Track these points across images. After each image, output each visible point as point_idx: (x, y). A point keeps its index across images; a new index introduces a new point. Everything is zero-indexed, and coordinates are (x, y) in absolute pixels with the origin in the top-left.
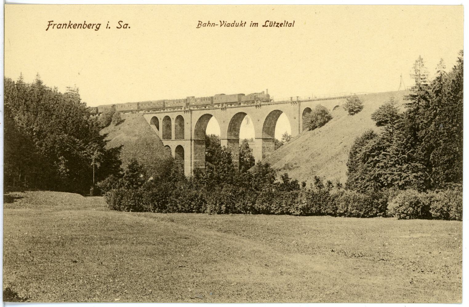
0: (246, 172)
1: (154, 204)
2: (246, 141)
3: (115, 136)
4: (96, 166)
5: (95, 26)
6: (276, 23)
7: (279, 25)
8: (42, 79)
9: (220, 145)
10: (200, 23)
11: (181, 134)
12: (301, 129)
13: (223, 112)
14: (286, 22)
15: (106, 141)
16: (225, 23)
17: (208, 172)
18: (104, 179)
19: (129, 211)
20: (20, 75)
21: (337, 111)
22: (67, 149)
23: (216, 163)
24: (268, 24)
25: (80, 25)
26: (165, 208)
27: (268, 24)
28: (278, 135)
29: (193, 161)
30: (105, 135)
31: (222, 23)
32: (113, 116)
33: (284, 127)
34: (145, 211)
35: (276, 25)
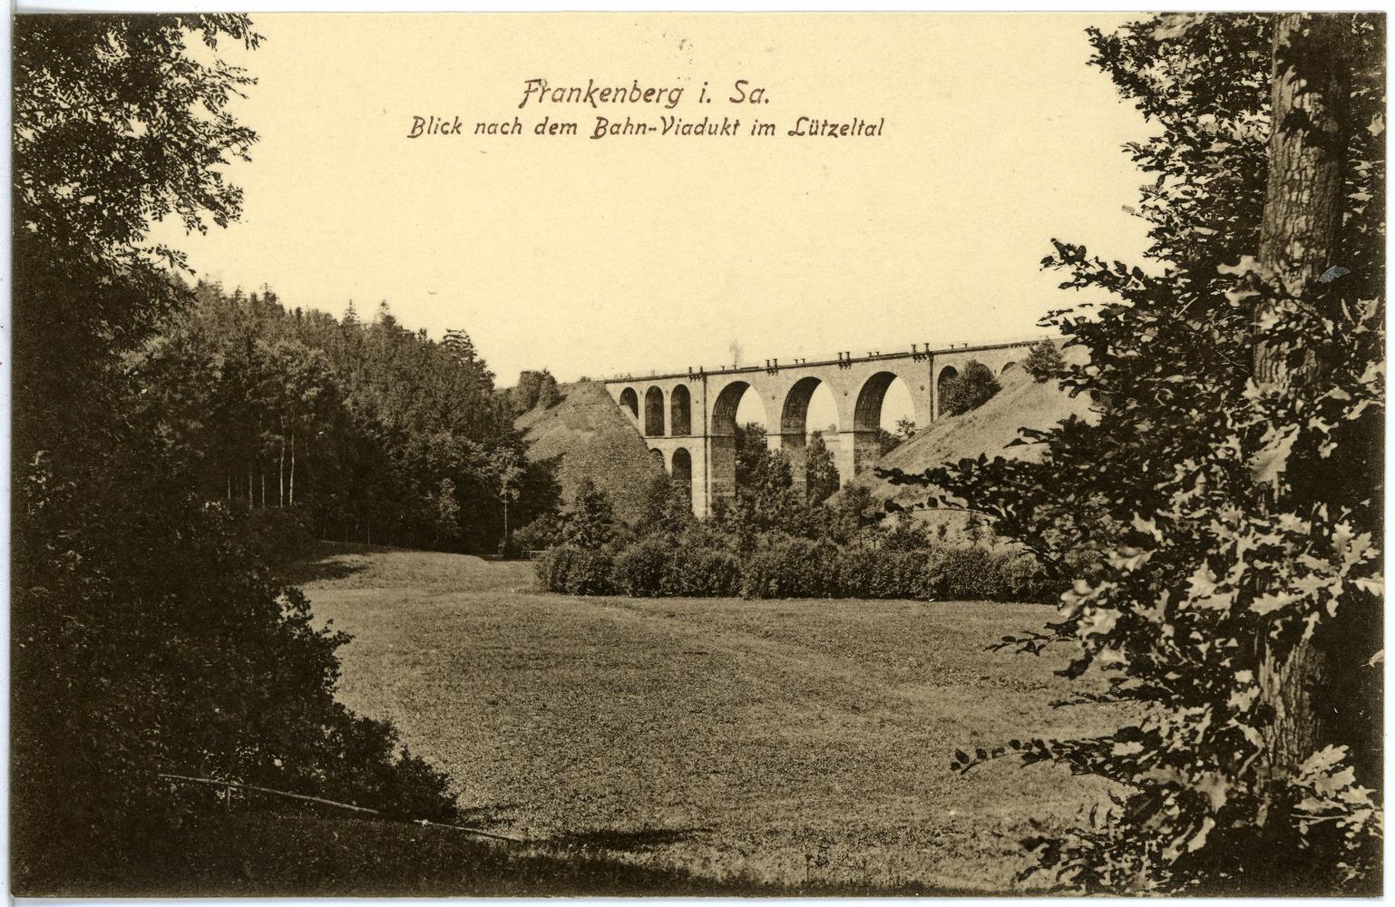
0: (821, 505)
1: (635, 579)
2: (817, 434)
3: (546, 434)
4: (509, 496)
5: (664, 97)
6: (829, 123)
7: (837, 131)
8: (392, 312)
9: (765, 446)
10: (603, 123)
11: (683, 424)
12: (936, 410)
13: (772, 377)
14: (859, 123)
15: (528, 442)
16: (677, 122)
17: (742, 507)
18: (526, 524)
19: (583, 594)
20: (348, 307)
21: (1011, 373)
22: (453, 464)
23: (758, 484)
24: (804, 126)
25: (622, 93)
26: (657, 586)
27: (804, 126)
28: (889, 421)
29: (710, 481)
30: (527, 430)
31: (669, 122)
32: (541, 389)
33: (898, 407)
34: (615, 593)
35: (828, 129)
